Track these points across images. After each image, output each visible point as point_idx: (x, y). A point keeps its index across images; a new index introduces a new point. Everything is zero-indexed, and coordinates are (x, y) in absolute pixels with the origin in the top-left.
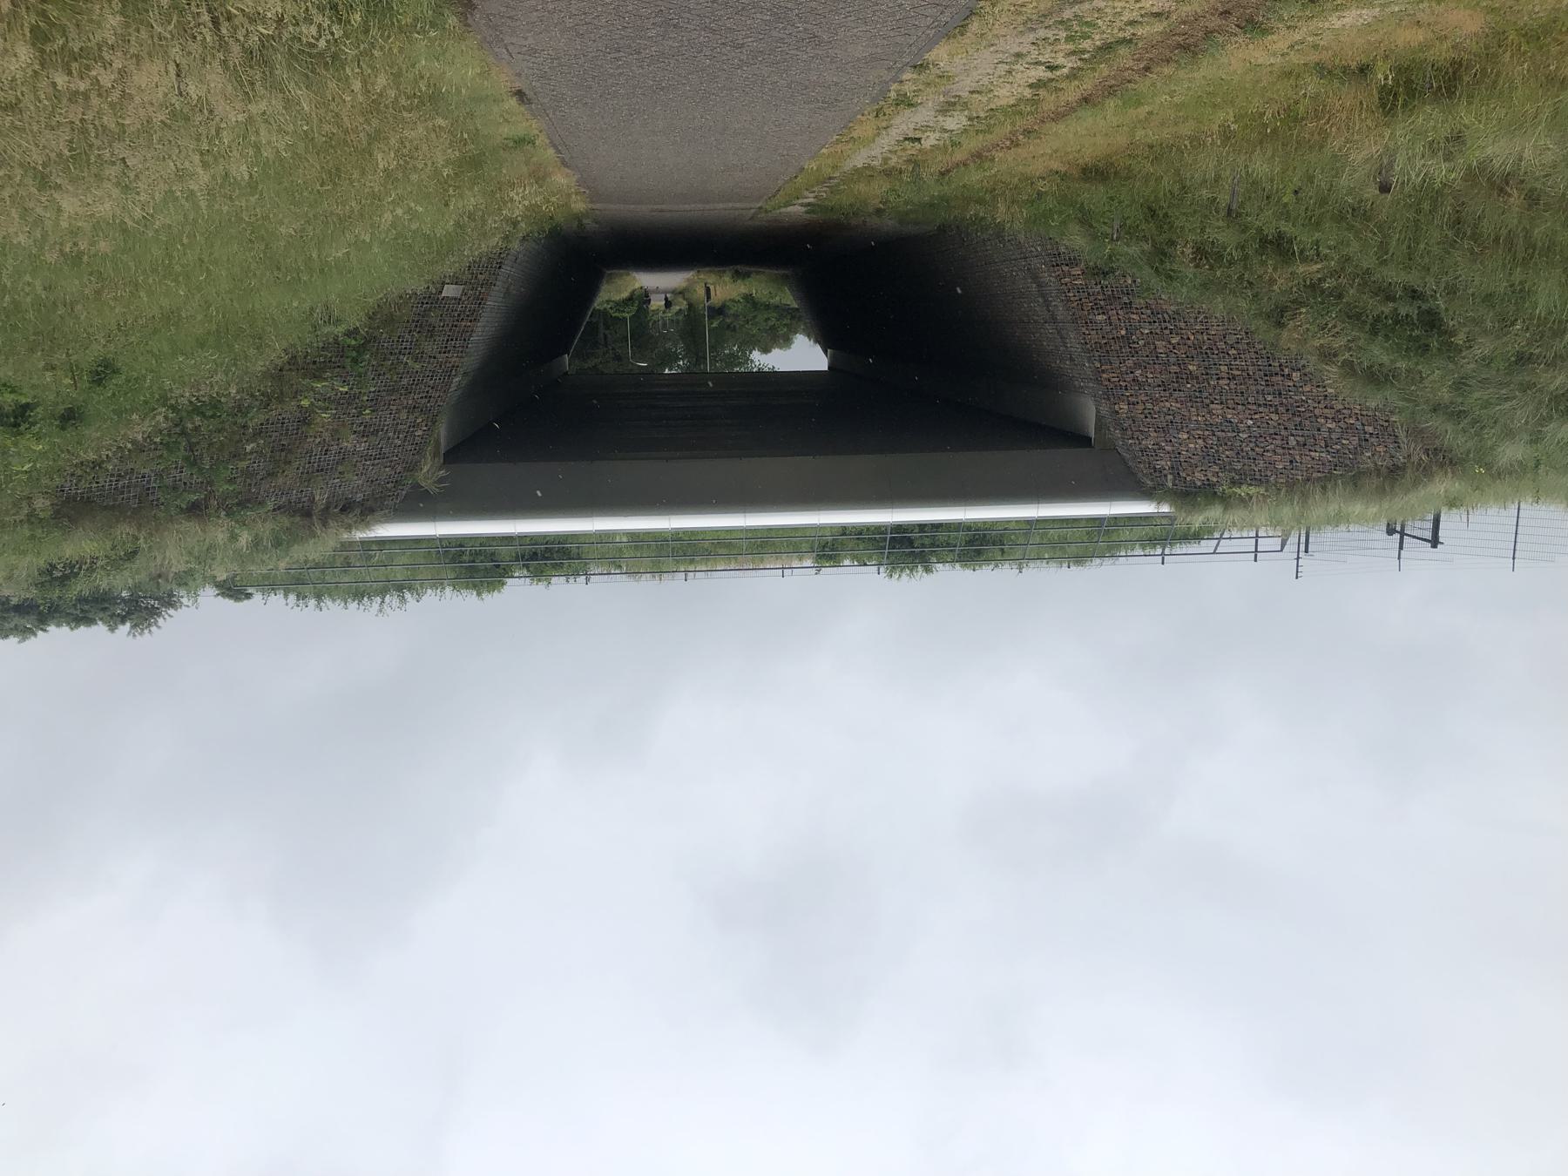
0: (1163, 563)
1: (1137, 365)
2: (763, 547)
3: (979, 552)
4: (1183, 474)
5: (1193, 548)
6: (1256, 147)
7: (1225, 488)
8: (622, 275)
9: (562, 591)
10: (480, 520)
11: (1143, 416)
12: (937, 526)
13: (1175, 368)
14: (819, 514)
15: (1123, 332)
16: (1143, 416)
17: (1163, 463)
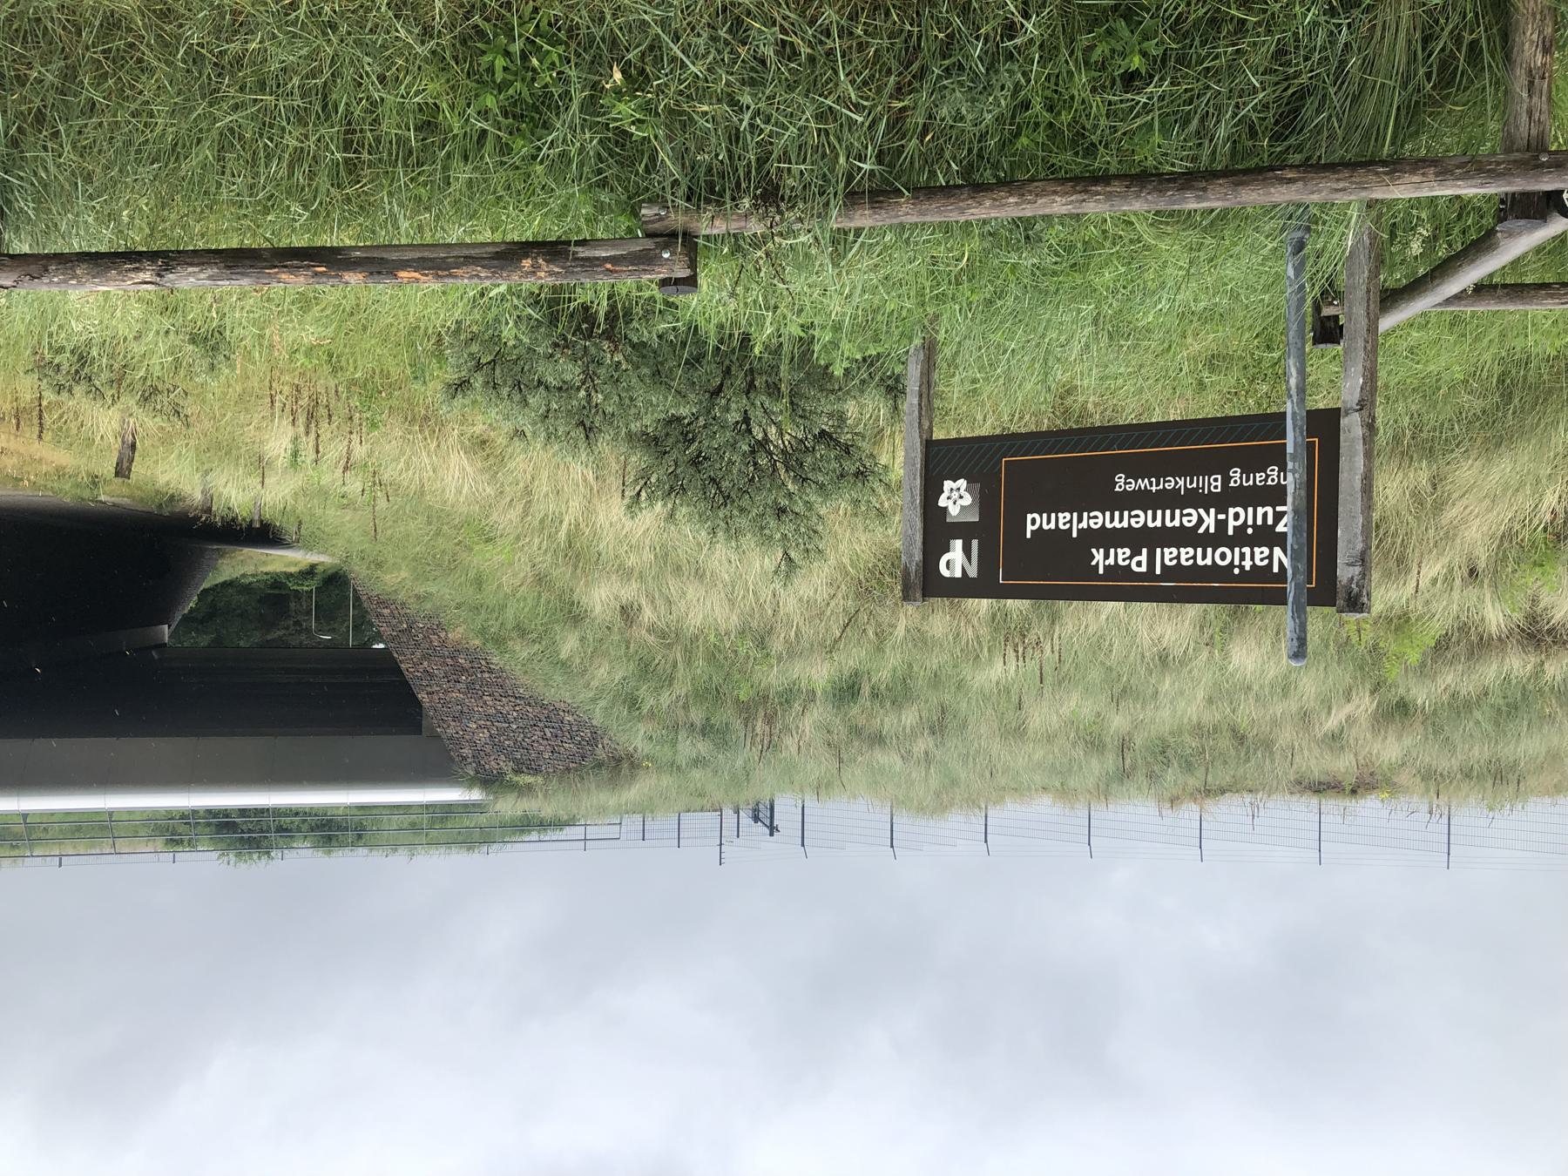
1: (424, 657)
2: (100, 829)
3: (330, 838)
4: (482, 762)
5: (558, 835)
6: (47, 407)
7: (510, 776)
8: (234, 551)
9: (349, 862)
10: (57, 795)
12: (261, 812)
13: (449, 661)
15: (405, 626)
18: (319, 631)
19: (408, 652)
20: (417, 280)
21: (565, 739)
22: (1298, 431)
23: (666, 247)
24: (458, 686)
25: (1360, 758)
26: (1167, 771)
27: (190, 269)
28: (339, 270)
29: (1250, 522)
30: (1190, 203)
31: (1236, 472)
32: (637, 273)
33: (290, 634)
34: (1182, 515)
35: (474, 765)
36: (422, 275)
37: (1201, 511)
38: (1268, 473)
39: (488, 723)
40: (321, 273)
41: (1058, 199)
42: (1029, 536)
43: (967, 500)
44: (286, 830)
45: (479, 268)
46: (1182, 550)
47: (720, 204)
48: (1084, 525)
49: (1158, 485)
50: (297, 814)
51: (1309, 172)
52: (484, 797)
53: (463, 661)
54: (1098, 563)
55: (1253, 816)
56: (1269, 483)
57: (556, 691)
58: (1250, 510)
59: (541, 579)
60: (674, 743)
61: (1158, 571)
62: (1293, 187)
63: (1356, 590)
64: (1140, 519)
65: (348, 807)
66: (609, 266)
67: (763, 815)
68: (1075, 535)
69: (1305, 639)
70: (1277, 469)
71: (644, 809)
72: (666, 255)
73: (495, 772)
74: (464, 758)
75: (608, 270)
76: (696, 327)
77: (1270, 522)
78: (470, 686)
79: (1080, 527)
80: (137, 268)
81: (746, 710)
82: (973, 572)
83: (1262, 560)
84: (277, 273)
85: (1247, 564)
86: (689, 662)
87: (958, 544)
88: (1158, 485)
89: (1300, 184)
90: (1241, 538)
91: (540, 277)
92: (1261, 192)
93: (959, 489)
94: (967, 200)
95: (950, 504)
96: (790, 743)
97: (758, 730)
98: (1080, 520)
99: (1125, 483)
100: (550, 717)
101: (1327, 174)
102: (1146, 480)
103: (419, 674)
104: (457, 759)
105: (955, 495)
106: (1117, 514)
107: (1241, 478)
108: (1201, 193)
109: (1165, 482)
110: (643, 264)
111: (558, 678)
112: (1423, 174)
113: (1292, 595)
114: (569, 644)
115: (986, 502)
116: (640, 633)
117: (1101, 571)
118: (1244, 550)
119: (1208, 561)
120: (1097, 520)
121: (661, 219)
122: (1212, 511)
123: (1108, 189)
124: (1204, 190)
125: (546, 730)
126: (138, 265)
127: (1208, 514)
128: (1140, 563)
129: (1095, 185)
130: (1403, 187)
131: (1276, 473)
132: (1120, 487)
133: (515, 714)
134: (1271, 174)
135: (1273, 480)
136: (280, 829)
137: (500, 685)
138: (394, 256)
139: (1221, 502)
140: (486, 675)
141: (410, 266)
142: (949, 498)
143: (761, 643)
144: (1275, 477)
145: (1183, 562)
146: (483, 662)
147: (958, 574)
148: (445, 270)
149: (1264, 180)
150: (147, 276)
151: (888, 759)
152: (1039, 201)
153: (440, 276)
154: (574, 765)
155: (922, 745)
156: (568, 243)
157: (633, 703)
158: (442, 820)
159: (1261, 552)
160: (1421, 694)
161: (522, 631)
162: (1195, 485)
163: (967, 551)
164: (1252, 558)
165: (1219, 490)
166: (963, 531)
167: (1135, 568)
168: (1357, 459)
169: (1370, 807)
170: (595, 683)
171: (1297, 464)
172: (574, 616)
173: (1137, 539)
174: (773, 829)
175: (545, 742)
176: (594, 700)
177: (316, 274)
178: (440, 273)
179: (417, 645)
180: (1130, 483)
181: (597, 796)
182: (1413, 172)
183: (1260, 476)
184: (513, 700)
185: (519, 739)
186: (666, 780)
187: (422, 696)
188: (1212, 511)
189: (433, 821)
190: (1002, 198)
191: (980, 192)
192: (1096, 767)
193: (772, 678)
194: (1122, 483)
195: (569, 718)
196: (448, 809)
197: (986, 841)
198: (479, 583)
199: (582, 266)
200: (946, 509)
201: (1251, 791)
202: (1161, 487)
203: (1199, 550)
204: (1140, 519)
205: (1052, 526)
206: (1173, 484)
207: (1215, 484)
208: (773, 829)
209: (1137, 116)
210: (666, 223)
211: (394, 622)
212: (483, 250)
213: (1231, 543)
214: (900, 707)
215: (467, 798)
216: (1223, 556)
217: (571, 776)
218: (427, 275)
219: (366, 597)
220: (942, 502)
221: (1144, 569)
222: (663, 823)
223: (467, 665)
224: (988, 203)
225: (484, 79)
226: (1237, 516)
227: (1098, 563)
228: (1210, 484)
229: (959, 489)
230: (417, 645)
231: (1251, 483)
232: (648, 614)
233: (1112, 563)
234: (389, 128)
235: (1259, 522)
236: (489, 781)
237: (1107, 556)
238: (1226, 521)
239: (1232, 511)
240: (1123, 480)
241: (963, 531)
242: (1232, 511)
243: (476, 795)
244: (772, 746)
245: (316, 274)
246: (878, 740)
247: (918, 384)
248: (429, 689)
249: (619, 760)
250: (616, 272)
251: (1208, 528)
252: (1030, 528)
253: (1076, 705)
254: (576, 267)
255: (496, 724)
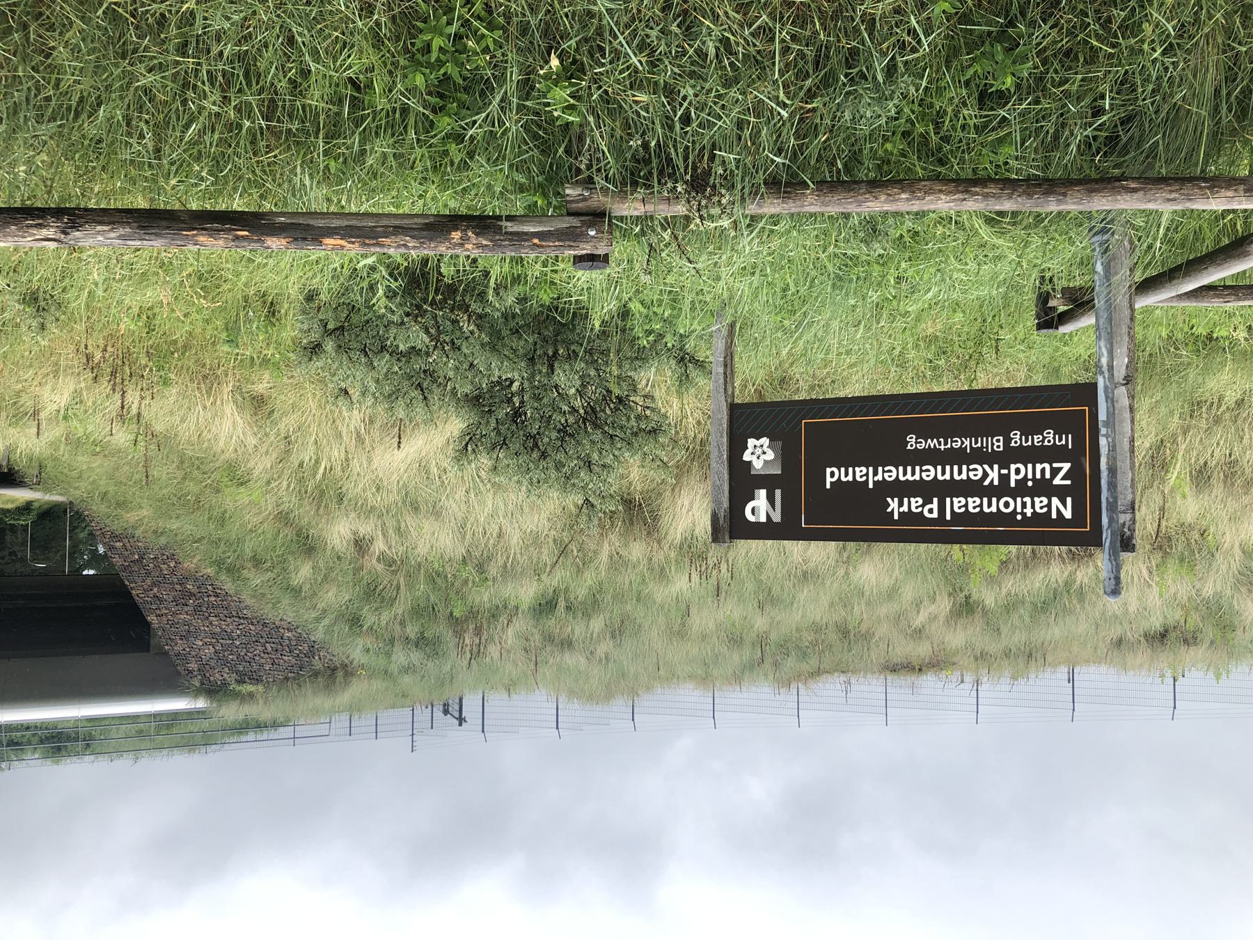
0: (350, 735)
1: (154, 584)
3: (59, 749)
5: (273, 734)
11: (168, 626)
13: (178, 587)
14: (79, 708)
15: (137, 557)
16: (168, 626)
17: (193, 666)
18: (34, 560)
19: (139, 580)
20: (342, 247)
21: (284, 653)
22: (1109, 401)
23: (591, 225)
24: (186, 609)
25: (935, 645)
26: (787, 660)
27: (99, 228)
28: (263, 234)
29: (1030, 476)
30: (1052, 206)
31: (1016, 434)
32: (562, 248)
33: (5, 564)
34: (921, 471)
35: (199, 677)
36: (349, 242)
37: (986, 467)
38: (1045, 435)
39: (214, 641)
40: (242, 236)
41: (943, 197)
42: (828, 486)
43: (770, 455)
44: (17, 744)
45: (408, 238)
46: (969, 499)
47: (648, 187)
48: (879, 477)
49: (946, 444)
50: (28, 728)
51: (1148, 184)
52: (209, 705)
53: (191, 587)
54: (893, 509)
55: (846, 691)
56: (1046, 443)
57: (285, 612)
58: (1030, 466)
59: (283, 518)
60: (389, 655)
61: (948, 517)
62: (1136, 196)
63: (1128, 533)
64: (930, 473)
65: (77, 720)
66: (536, 241)
67: (454, 708)
68: (871, 486)
69: (1119, 578)
70: (1052, 432)
71: (354, 709)
72: (592, 233)
73: (219, 683)
74: (191, 672)
75: (534, 244)
76: (1093, 288)
77: (1048, 476)
78: (197, 610)
79: (876, 479)
80: (39, 224)
81: (457, 625)
82: (776, 517)
83: (1041, 508)
84: (194, 236)
85: (1029, 511)
86: (410, 587)
87: (762, 493)
88: (946, 444)
89: (1141, 194)
90: (1021, 489)
91: (411, 251)
92: (1110, 198)
93: (762, 446)
94: (865, 194)
95: (754, 459)
96: (493, 650)
97: (467, 641)
98: (875, 474)
99: (916, 443)
100: (270, 633)
101: (1162, 186)
102: (935, 440)
103: (149, 599)
104: (183, 673)
105: (759, 451)
106: (909, 468)
107: (1054, 438)
108: (1061, 197)
109: (952, 442)
110: (569, 240)
111: (286, 601)
112: (1235, 190)
113: (1108, 541)
114: (303, 572)
115: (787, 456)
116: (371, 563)
117: (896, 517)
118: (1025, 499)
119: (994, 509)
120: (892, 473)
121: (585, 199)
122: (996, 467)
123: (985, 190)
124: (1065, 195)
125: (267, 645)
126: (40, 221)
127: (992, 470)
128: (932, 510)
129: (974, 187)
130: (1219, 200)
131: (1018, 437)
132: (912, 446)
133: (238, 632)
134: (1117, 184)
135: (1049, 441)
136: (12, 743)
137: (226, 606)
138: (320, 223)
139: (1003, 459)
140: (213, 599)
141: (337, 234)
142: (752, 454)
143: (481, 568)
144: (1051, 439)
145: (971, 509)
146: (210, 588)
147: (763, 519)
148: (373, 238)
149: (1113, 188)
150: (50, 233)
151: (572, 660)
152: (927, 198)
153: (368, 245)
154: (292, 675)
155: (603, 648)
156: (499, 218)
157: (355, 621)
158: (168, 727)
159: (1040, 502)
160: (989, 598)
161: (257, 562)
162: (979, 445)
163: (771, 499)
164: (1033, 506)
165: (1001, 449)
166: (768, 482)
167: (926, 514)
168: (1125, 424)
169: (929, 682)
170: (321, 606)
171: (1110, 430)
172: (307, 545)
173: (927, 490)
174: (461, 720)
175: (266, 656)
176: (318, 620)
177: (237, 238)
178: (367, 241)
179: (148, 574)
180: (921, 442)
181: (312, 699)
182: (1228, 188)
183: (1037, 439)
184: (237, 619)
185: (242, 654)
186: (378, 684)
187: (152, 618)
188: (996, 467)
189: (158, 728)
190: (896, 194)
191: (876, 187)
192: (737, 658)
193: (483, 597)
194: (912, 442)
195: (287, 634)
196: (175, 716)
197: (633, 720)
198: (222, 521)
199: (510, 240)
200: (750, 463)
201: (843, 672)
202: (949, 446)
203: (985, 500)
204: (930, 473)
205: (850, 478)
206: (959, 444)
207: (998, 444)
208: (461, 720)
209: (993, 129)
210: (589, 203)
211: (126, 553)
212: (412, 221)
213: (1014, 494)
214: (589, 617)
215: (193, 707)
216: (1007, 505)
217: (289, 683)
218: (353, 243)
219: (99, 532)
220: (747, 457)
221: (935, 515)
222: (364, 722)
223: (195, 590)
224: (883, 198)
225: (418, 57)
226: (1018, 471)
227: (893, 509)
228: (993, 444)
229: (762, 446)
230: (148, 574)
231: (1030, 443)
232: (379, 546)
233: (906, 510)
234: (316, 98)
235: (1038, 476)
236: (214, 691)
237: (901, 504)
238: (1008, 475)
239: (1013, 467)
240: (914, 440)
241: (768, 482)
242: (1013, 467)
243: (201, 703)
244: (477, 653)
245: (237, 238)
246: (567, 644)
247: (723, 356)
248: (158, 612)
249: (334, 669)
250: (542, 247)
251: (992, 480)
252: (829, 480)
253: (731, 611)
254: (504, 240)
255: (221, 641)
